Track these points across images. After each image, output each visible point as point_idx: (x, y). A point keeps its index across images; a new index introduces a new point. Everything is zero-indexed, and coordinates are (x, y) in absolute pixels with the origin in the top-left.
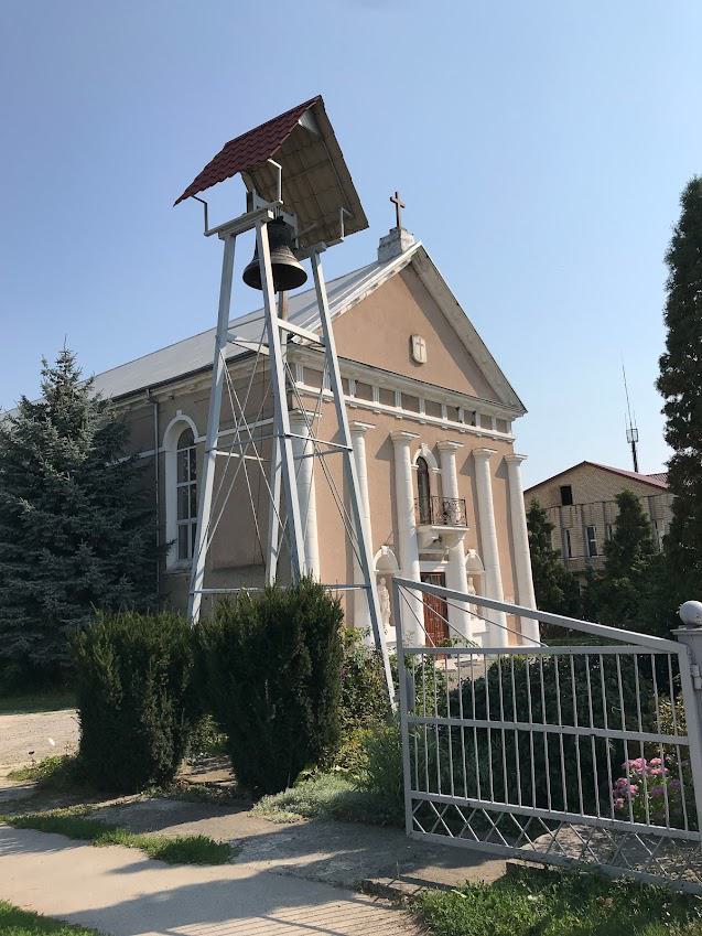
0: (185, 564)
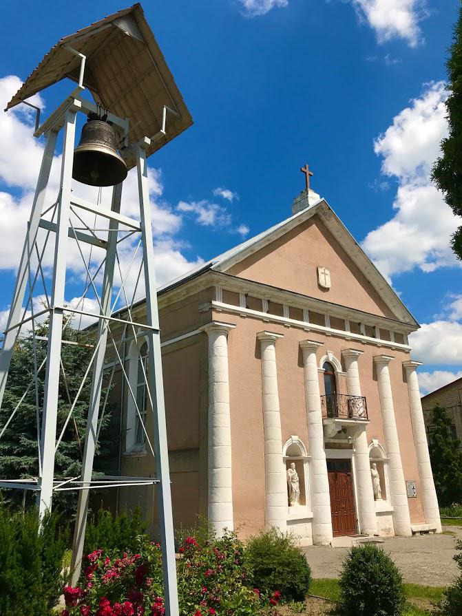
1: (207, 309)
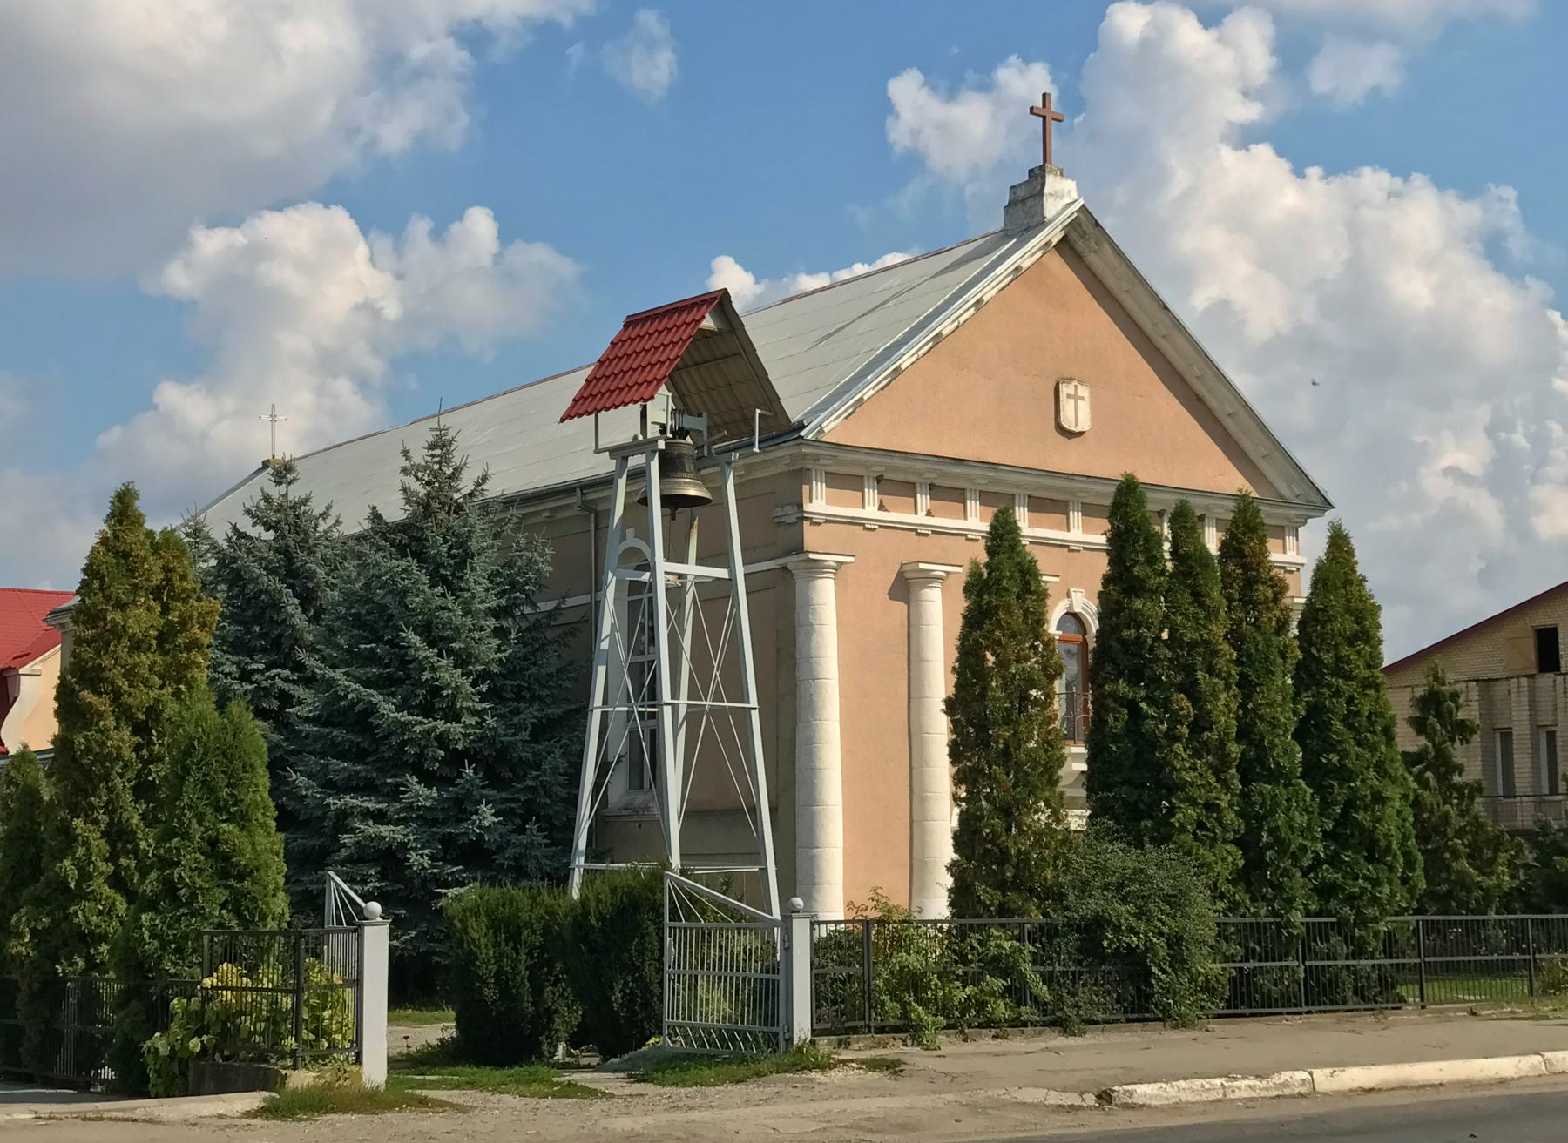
0: (639, 799)
1: (793, 519)
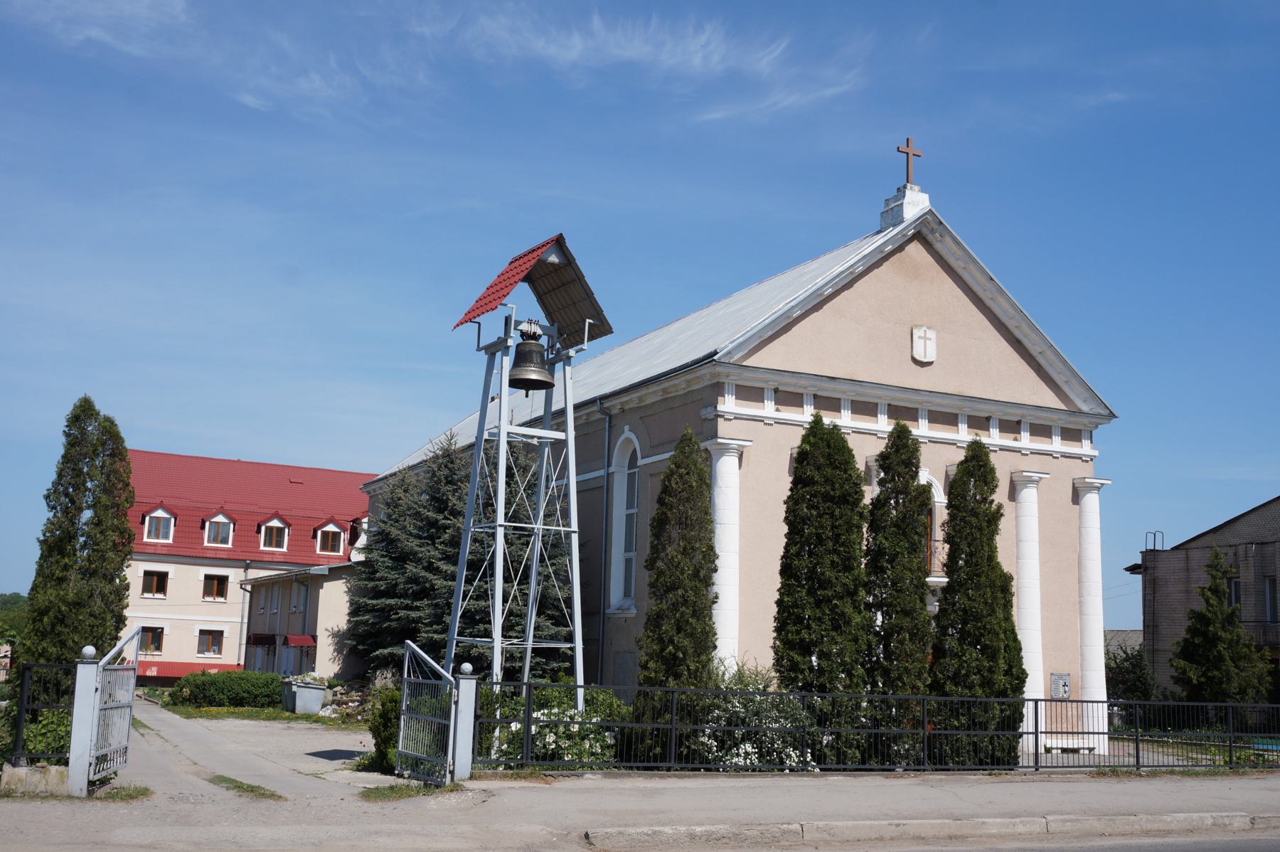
1: (712, 416)
